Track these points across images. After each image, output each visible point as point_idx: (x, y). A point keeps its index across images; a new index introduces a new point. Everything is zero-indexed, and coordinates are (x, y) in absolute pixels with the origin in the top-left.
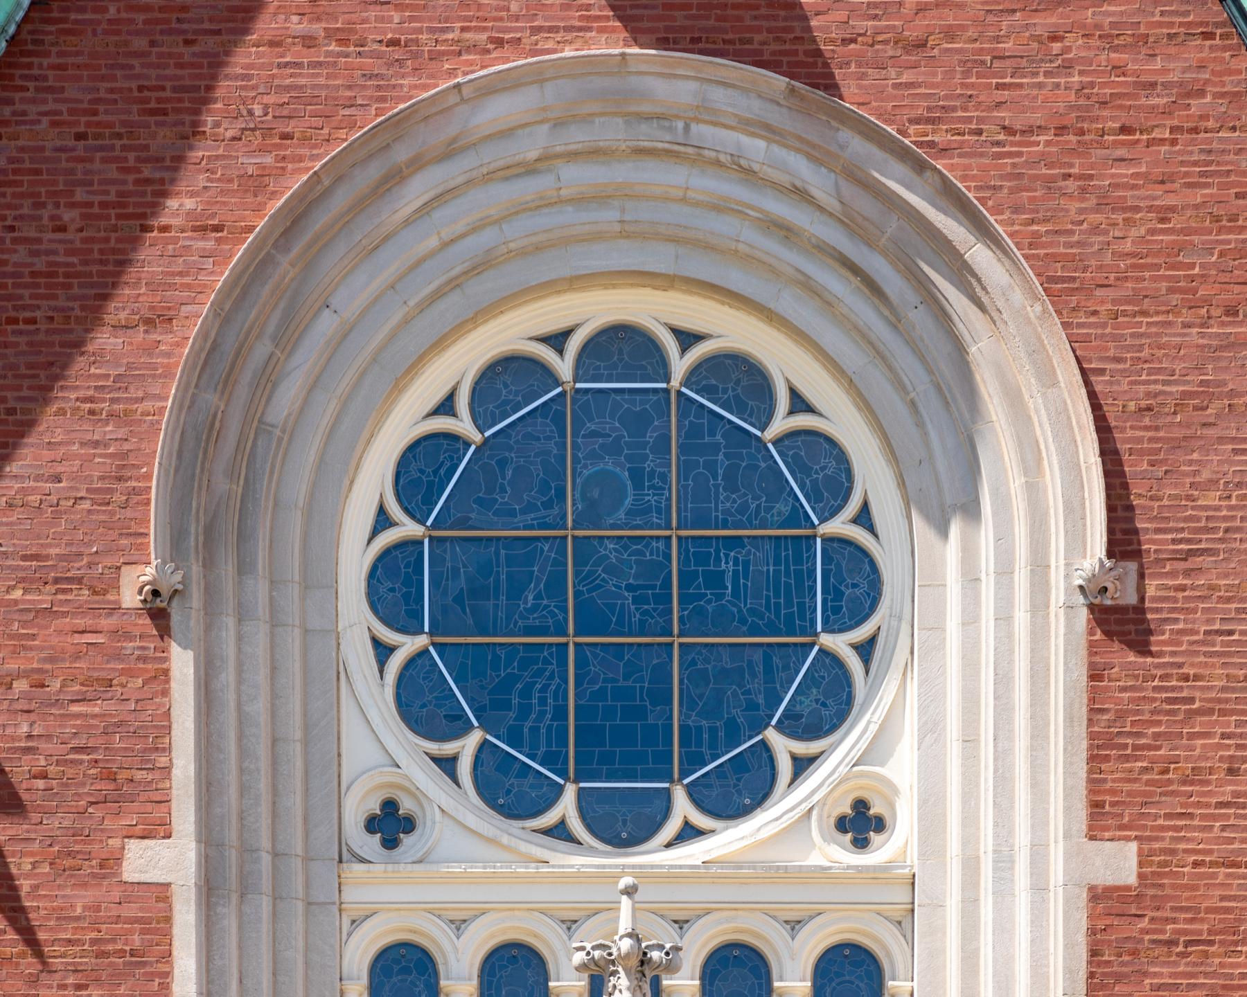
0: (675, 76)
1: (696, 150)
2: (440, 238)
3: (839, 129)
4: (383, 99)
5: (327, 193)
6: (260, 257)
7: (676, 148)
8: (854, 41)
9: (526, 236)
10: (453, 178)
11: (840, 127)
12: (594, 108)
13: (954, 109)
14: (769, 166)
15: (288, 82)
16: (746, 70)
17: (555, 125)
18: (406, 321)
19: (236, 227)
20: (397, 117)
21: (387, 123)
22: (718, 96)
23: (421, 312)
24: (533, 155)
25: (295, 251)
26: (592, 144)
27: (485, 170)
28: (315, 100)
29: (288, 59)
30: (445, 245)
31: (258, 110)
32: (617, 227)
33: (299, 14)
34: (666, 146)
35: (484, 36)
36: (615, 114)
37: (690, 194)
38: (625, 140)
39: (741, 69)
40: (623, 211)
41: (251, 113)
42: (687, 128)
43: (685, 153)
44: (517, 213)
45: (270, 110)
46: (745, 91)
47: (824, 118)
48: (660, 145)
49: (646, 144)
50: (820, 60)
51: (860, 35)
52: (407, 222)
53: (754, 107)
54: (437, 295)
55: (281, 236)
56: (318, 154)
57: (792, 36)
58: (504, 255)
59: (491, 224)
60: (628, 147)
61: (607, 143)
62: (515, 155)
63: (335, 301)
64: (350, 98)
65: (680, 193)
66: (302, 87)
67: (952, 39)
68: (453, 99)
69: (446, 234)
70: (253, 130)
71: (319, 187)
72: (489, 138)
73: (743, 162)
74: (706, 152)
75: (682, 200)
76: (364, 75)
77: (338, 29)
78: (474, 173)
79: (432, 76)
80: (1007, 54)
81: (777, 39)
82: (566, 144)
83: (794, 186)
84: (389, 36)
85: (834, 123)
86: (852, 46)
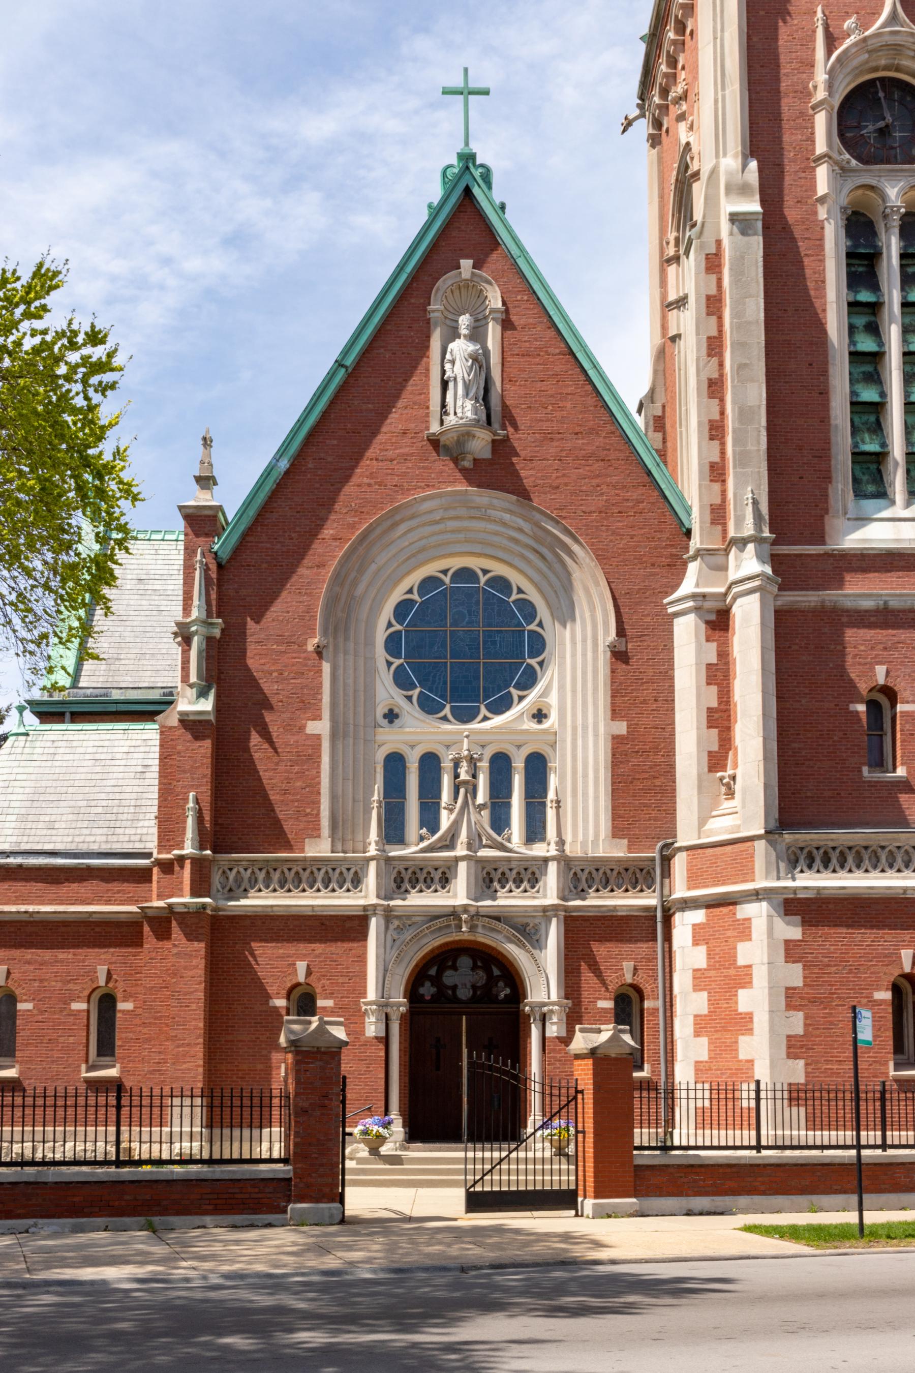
5: (374, 529)
18: (398, 566)
22: (495, 501)
24: (438, 518)
30: (411, 544)
31: (353, 505)
52: (399, 538)
72: (425, 513)
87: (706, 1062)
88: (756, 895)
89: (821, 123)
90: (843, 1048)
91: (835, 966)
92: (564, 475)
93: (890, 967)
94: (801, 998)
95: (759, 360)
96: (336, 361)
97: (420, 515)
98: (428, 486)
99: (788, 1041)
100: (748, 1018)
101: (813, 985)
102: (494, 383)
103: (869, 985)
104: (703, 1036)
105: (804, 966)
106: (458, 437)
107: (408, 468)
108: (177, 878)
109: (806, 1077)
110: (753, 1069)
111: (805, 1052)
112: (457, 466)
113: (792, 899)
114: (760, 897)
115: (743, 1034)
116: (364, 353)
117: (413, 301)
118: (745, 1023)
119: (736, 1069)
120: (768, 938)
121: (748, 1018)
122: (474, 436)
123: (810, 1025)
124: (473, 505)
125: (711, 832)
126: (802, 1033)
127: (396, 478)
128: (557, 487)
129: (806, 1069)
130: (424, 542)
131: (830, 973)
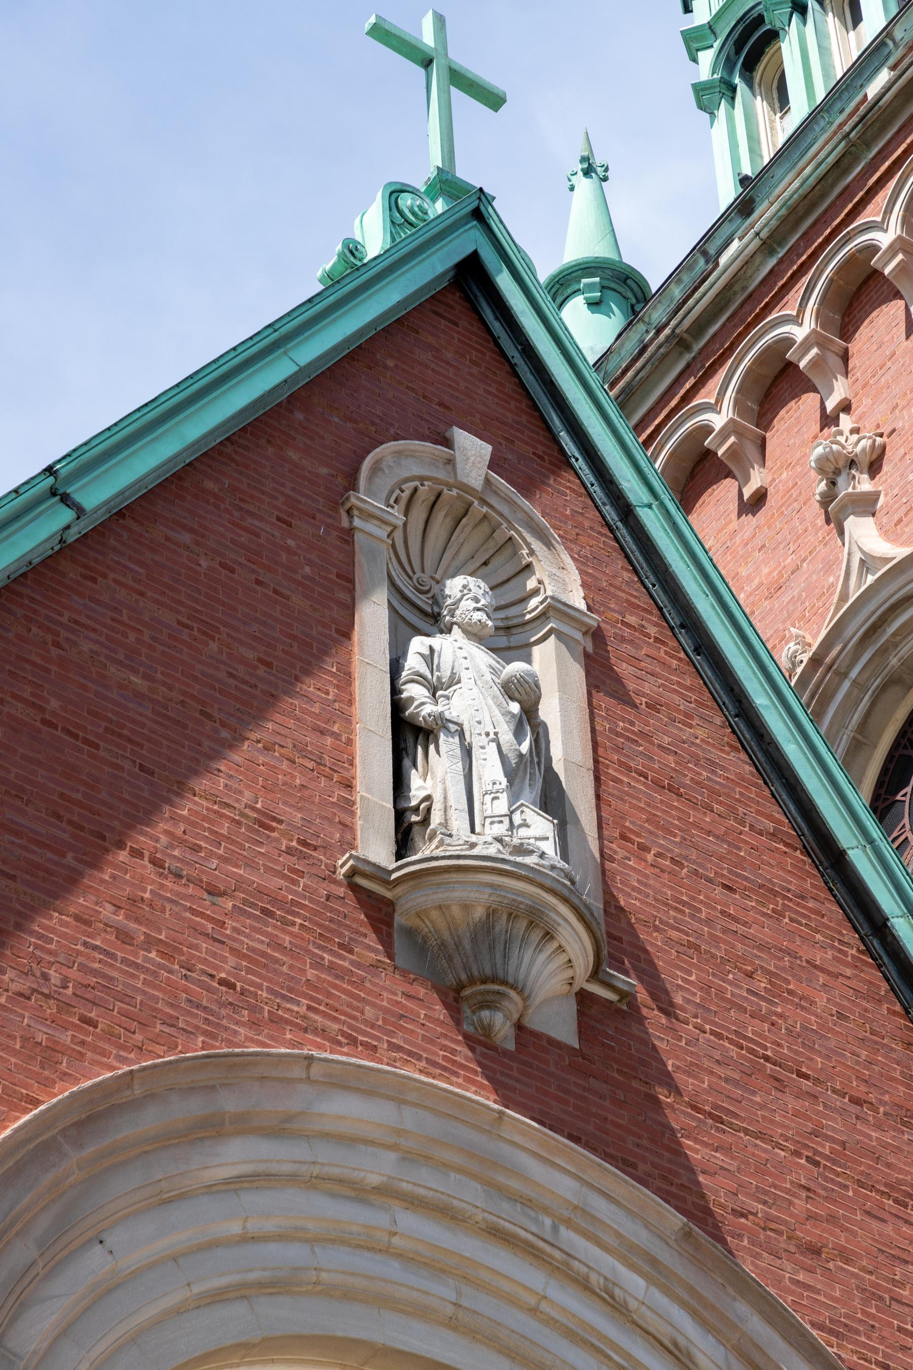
0: (553, 1164)
1: (564, 1256)
2: (244, 1228)
3: (735, 1299)
4: (213, 1036)
5: (135, 1105)
6: (44, 1137)
7: (541, 1244)
8: (743, 1215)
9: (343, 1272)
10: (278, 1162)
11: (738, 1297)
12: (456, 1159)
13: (857, 1332)
14: (649, 1307)
15: (96, 966)
16: (638, 1190)
17: (404, 1159)
18: (179, 1311)
19: (15, 1091)
20: (236, 1059)
21: (222, 1059)
22: (600, 1206)
23: (197, 1308)
24: (374, 1179)
25: (89, 1150)
26: (444, 1197)
27: (316, 1170)
28: (127, 999)
29: (98, 943)
30: (247, 1239)
31: (55, 977)
32: (449, 1310)
33: (114, 905)
34: (530, 1237)
35: (336, 1027)
36: (474, 1177)
37: (544, 1306)
38: (484, 1211)
39: (633, 1186)
40: (459, 1294)
41: (45, 977)
42: (555, 1229)
43: (550, 1256)
44: (333, 1241)
45: (71, 985)
46: (629, 1212)
47: (720, 1280)
48: (523, 1234)
49: (507, 1225)
50: (710, 1220)
51: (752, 1213)
52: (210, 1189)
53: (641, 1236)
54: (219, 1297)
55: (71, 1125)
56: (127, 1058)
57: (679, 1182)
58: (309, 1283)
59: (307, 1241)
60: (484, 1219)
61: (463, 1205)
62: (354, 1169)
63: (111, 1240)
64: (171, 1017)
65: (533, 1302)
66: (112, 979)
67: (847, 1261)
68: (298, 1072)
69: (253, 1226)
70: (47, 996)
71: (128, 1093)
72: (327, 1136)
73: (617, 1292)
74: (576, 1264)
75: (530, 1310)
76: (190, 1001)
77: (160, 940)
78: (304, 1168)
79: (272, 1038)
80: (904, 1301)
81: (663, 1177)
82: (414, 1184)
83: (676, 1344)
84: (223, 975)
85: (730, 1290)
86: (743, 1220)
89: (465, 894)
92: (832, 1219)
96: (49, 470)
97: (307, 1137)
98: (353, 1041)
102: (577, 821)
106: (491, 913)
107: (279, 947)
112: (458, 1022)
116: (120, 514)
117: (293, 455)
122: (548, 936)
124: (514, 1184)
127: (232, 961)
128: (815, 1251)
130: (295, 1253)
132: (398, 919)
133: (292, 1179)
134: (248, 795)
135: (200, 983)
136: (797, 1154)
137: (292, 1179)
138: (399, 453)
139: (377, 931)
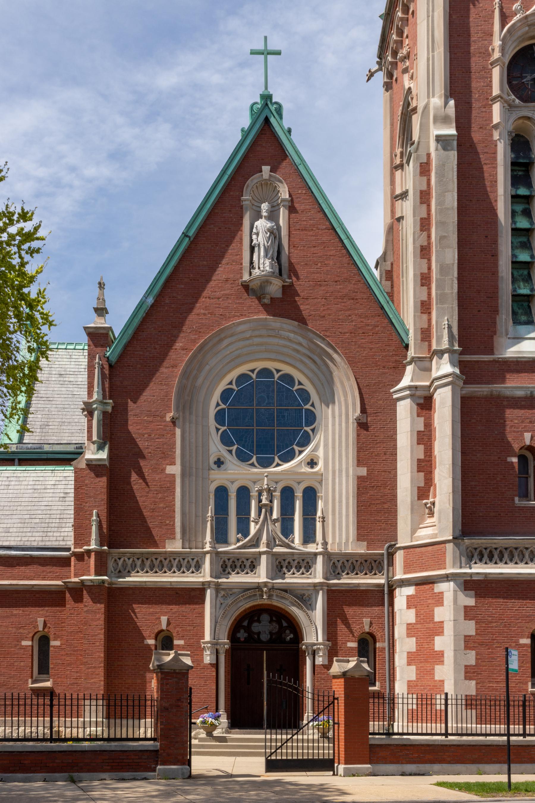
18: (223, 367)
24: (248, 336)
30: (231, 353)
31: (194, 327)
52: (223, 349)
67: (330, 316)
72: (240, 333)
87: (415, 681)
88: (447, 578)
90: (500, 674)
91: (495, 622)
92: (328, 309)
93: (530, 624)
94: (474, 642)
95: (453, 234)
96: (183, 233)
99: (465, 669)
100: (441, 654)
101: (482, 634)
103: (517, 635)
104: (413, 665)
105: (476, 622)
106: (261, 283)
108: (87, 564)
109: (476, 691)
110: (444, 686)
111: (476, 676)
112: (260, 303)
113: (469, 580)
114: (449, 579)
115: (437, 664)
116: (201, 228)
117: (232, 193)
118: (439, 657)
119: (433, 686)
120: (454, 604)
121: (441, 654)
122: (271, 283)
123: (479, 659)
125: (420, 538)
126: (474, 664)
129: (476, 686)
131: (492, 627)
132: (250, 287)
133: (235, 342)
134: (224, 276)
135: (218, 317)
136: (322, 299)
137: (235, 342)
138: (252, 180)
139: (246, 292)
